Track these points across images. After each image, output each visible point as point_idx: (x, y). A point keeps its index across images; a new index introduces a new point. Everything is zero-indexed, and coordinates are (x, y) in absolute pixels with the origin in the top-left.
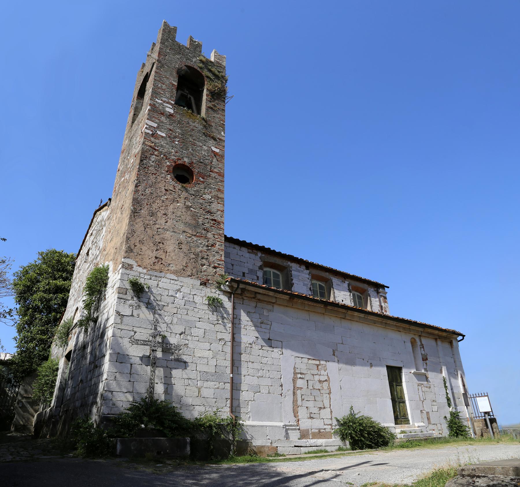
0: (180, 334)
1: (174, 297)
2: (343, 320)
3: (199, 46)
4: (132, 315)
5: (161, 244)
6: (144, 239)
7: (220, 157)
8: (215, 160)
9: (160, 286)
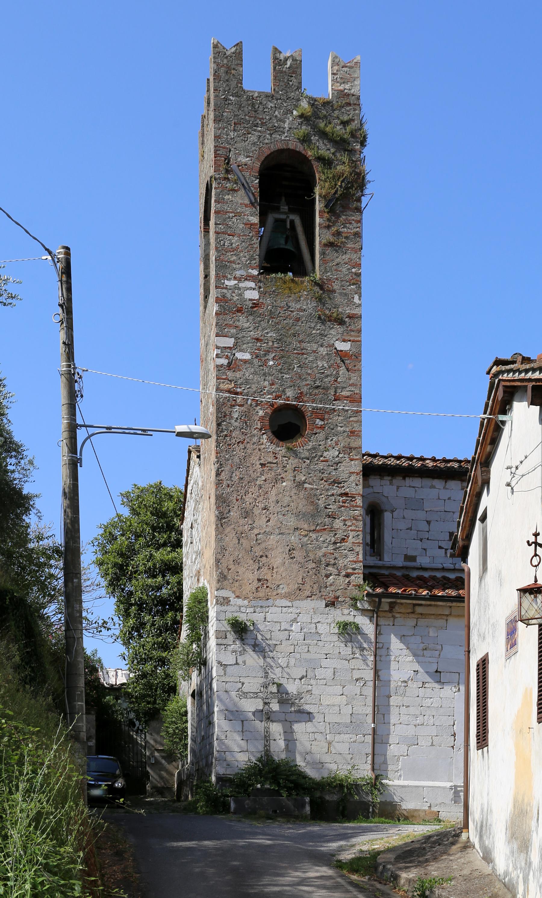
0: (301, 679)
1: (289, 630)
4: (237, 664)
5: (264, 558)
7: (351, 360)
8: (342, 370)
9: (268, 619)
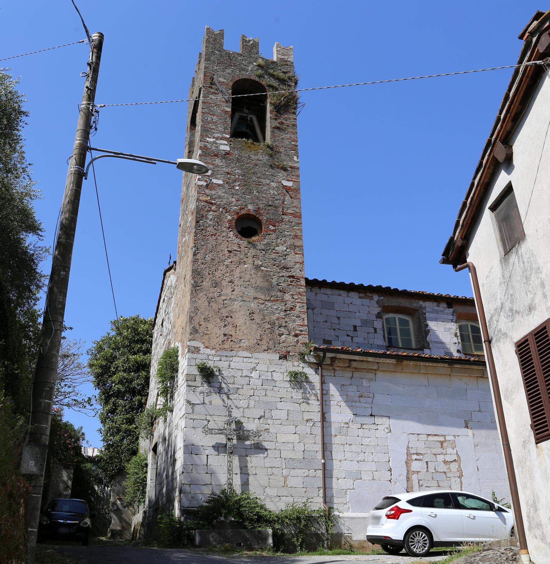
0: (259, 419)
1: (249, 377)
2: (480, 379)
3: (255, 45)
5: (229, 318)
6: (210, 316)
8: (287, 198)
9: (232, 367)
